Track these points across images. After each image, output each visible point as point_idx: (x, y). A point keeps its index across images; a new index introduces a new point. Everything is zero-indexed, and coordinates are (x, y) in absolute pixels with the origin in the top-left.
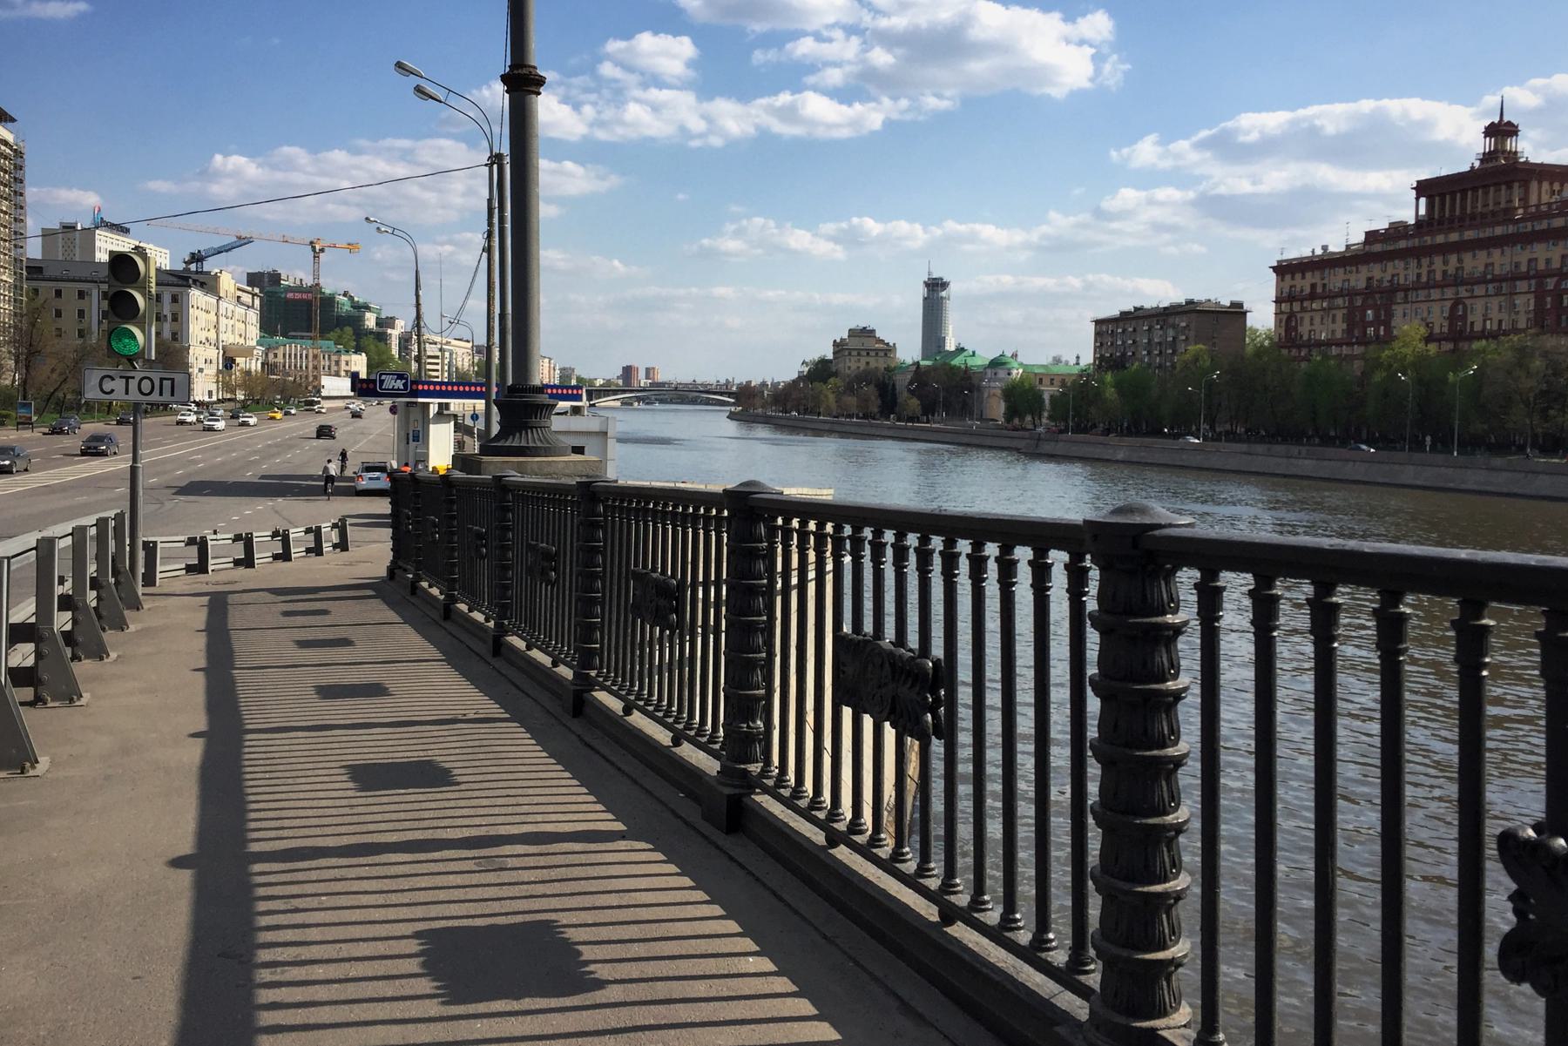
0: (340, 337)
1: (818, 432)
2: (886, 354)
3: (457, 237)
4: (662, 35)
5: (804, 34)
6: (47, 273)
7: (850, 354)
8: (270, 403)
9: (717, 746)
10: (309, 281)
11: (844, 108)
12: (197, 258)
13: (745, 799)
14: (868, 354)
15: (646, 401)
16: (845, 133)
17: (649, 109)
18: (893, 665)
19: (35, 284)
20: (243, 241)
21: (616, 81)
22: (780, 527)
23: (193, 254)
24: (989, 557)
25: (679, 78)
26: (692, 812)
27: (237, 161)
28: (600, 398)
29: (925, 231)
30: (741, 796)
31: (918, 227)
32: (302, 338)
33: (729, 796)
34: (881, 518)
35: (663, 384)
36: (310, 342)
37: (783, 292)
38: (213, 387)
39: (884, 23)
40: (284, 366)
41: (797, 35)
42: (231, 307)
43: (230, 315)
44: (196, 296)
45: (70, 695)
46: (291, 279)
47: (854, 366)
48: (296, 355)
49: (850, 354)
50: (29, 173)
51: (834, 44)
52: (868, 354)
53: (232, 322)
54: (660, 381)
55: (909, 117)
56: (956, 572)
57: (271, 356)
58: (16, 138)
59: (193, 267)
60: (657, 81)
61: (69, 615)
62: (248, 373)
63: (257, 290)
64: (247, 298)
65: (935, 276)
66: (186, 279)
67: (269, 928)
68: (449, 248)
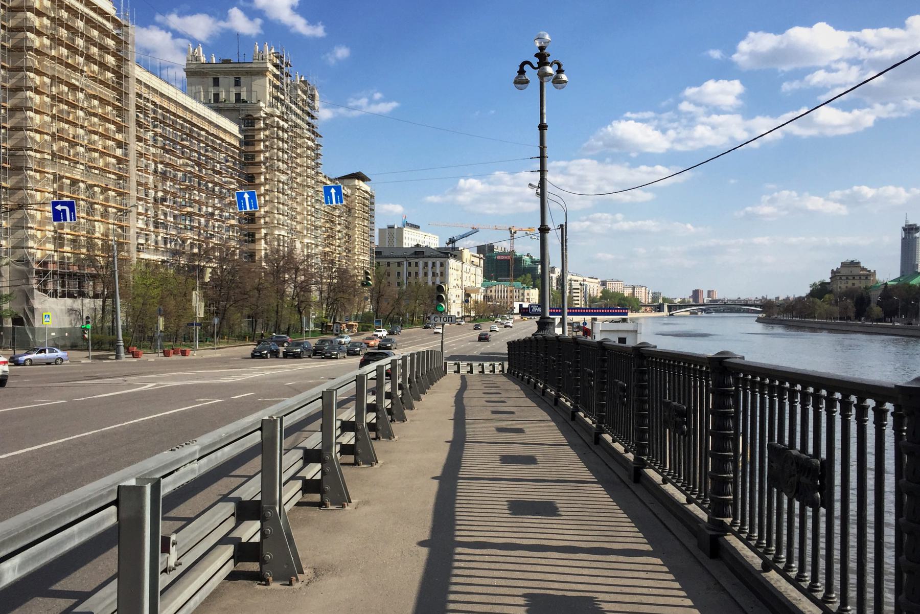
0: (524, 280)
1: (813, 330)
2: (867, 278)
3: (591, 216)
4: (721, 81)
5: (820, 68)
6: (383, 254)
7: (841, 278)
8: (488, 317)
9: (707, 506)
10: (508, 249)
11: (846, 114)
12: (452, 241)
13: (720, 539)
14: (854, 278)
15: (706, 311)
16: (846, 131)
17: (710, 128)
18: (797, 464)
19: (379, 260)
20: (475, 231)
21: (690, 113)
22: (812, 394)
23: (450, 239)
24: (869, 406)
25: (731, 106)
26: (691, 543)
27: (472, 181)
28: (676, 310)
29: (907, 191)
30: (719, 536)
31: (902, 190)
32: (505, 281)
33: (711, 535)
34: (864, 390)
35: (717, 301)
36: (509, 283)
37: (803, 239)
38: (460, 310)
39: (877, 54)
40: (495, 297)
41: (813, 70)
42: (469, 267)
43: (468, 271)
44: (452, 262)
45: (389, 436)
46: (500, 248)
47: (843, 286)
48: (501, 290)
49: (841, 278)
50: (376, 200)
51: (840, 73)
52: (854, 278)
53: (468, 275)
54: (717, 299)
55: (895, 115)
56: (835, 410)
57: (489, 291)
58: (371, 189)
59: (450, 246)
60: (718, 110)
61: (390, 401)
62: (476, 302)
63: (482, 256)
64: (476, 261)
65: (910, 223)
66: (447, 254)
67: (459, 530)
68: (587, 223)
